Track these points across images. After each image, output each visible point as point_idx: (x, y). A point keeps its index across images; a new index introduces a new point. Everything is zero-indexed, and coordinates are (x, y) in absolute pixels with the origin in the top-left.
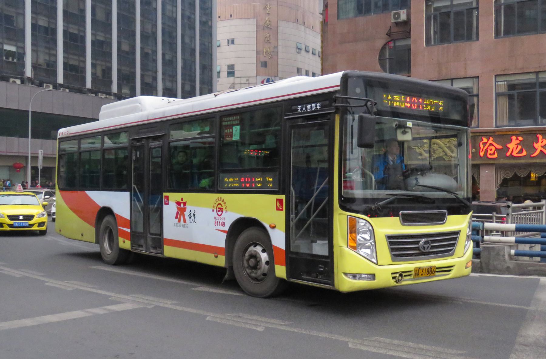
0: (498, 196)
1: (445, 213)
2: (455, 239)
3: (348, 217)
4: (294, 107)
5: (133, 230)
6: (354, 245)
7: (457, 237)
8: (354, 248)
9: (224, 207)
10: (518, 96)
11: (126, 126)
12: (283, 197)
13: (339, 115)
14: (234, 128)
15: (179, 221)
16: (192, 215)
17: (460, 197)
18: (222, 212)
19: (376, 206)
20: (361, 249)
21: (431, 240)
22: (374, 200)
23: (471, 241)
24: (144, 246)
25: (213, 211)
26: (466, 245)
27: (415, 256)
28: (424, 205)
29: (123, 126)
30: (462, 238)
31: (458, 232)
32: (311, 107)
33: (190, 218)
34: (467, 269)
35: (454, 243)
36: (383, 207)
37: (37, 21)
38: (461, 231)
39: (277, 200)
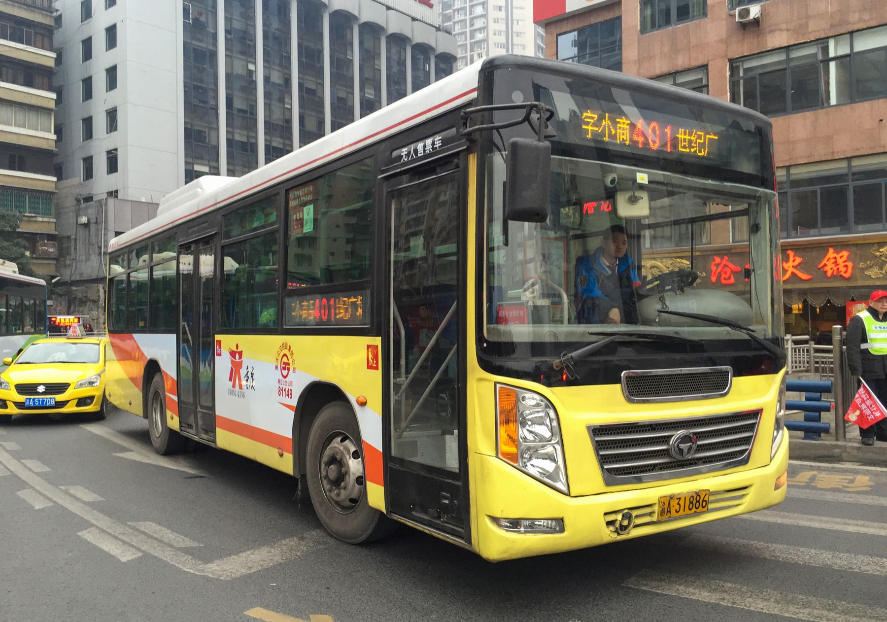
0: (28, 321)
1: (728, 372)
2: (751, 427)
3: (498, 386)
4: (395, 154)
5: (182, 399)
6: (513, 450)
7: (754, 424)
8: (511, 458)
9: (290, 362)
10: (822, 194)
11: (175, 224)
12: (377, 341)
13: (476, 154)
14: (305, 209)
15: (234, 386)
16: (249, 375)
17: (760, 336)
18: (289, 369)
19: (563, 359)
20: (530, 459)
21: (695, 434)
22: (559, 347)
23: (785, 428)
24: (194, 428)
25: (277, 368)
26: (774, 439)
27: (661, 469)
28: (678, 356)
29: (170, 226)
30: (766, 423)
31: (758, 413)
32: (425, 146)
33: (247, 380)
34: (777, 491)
35: (748, 437)
36: (579, 362)
37: (233, 136)
38: (764, 411)
39: (369, 347)
